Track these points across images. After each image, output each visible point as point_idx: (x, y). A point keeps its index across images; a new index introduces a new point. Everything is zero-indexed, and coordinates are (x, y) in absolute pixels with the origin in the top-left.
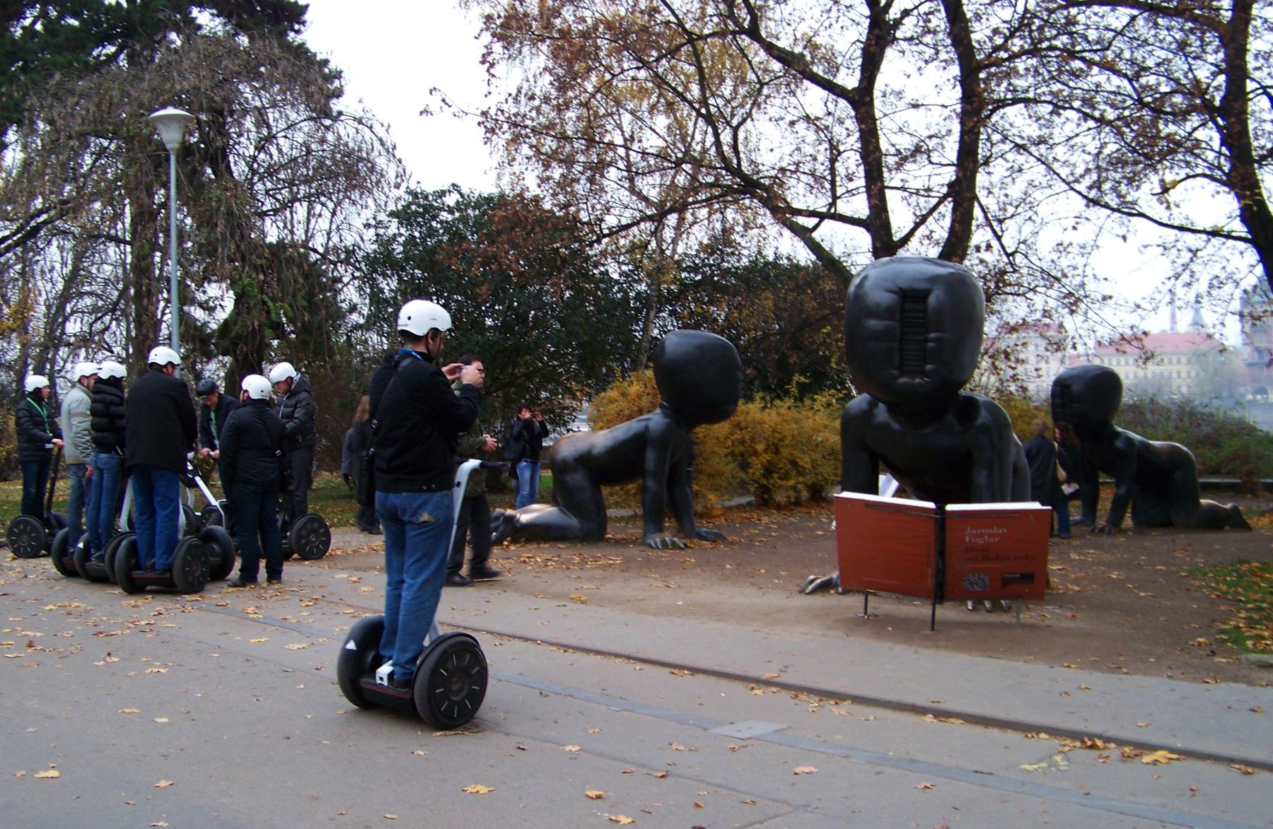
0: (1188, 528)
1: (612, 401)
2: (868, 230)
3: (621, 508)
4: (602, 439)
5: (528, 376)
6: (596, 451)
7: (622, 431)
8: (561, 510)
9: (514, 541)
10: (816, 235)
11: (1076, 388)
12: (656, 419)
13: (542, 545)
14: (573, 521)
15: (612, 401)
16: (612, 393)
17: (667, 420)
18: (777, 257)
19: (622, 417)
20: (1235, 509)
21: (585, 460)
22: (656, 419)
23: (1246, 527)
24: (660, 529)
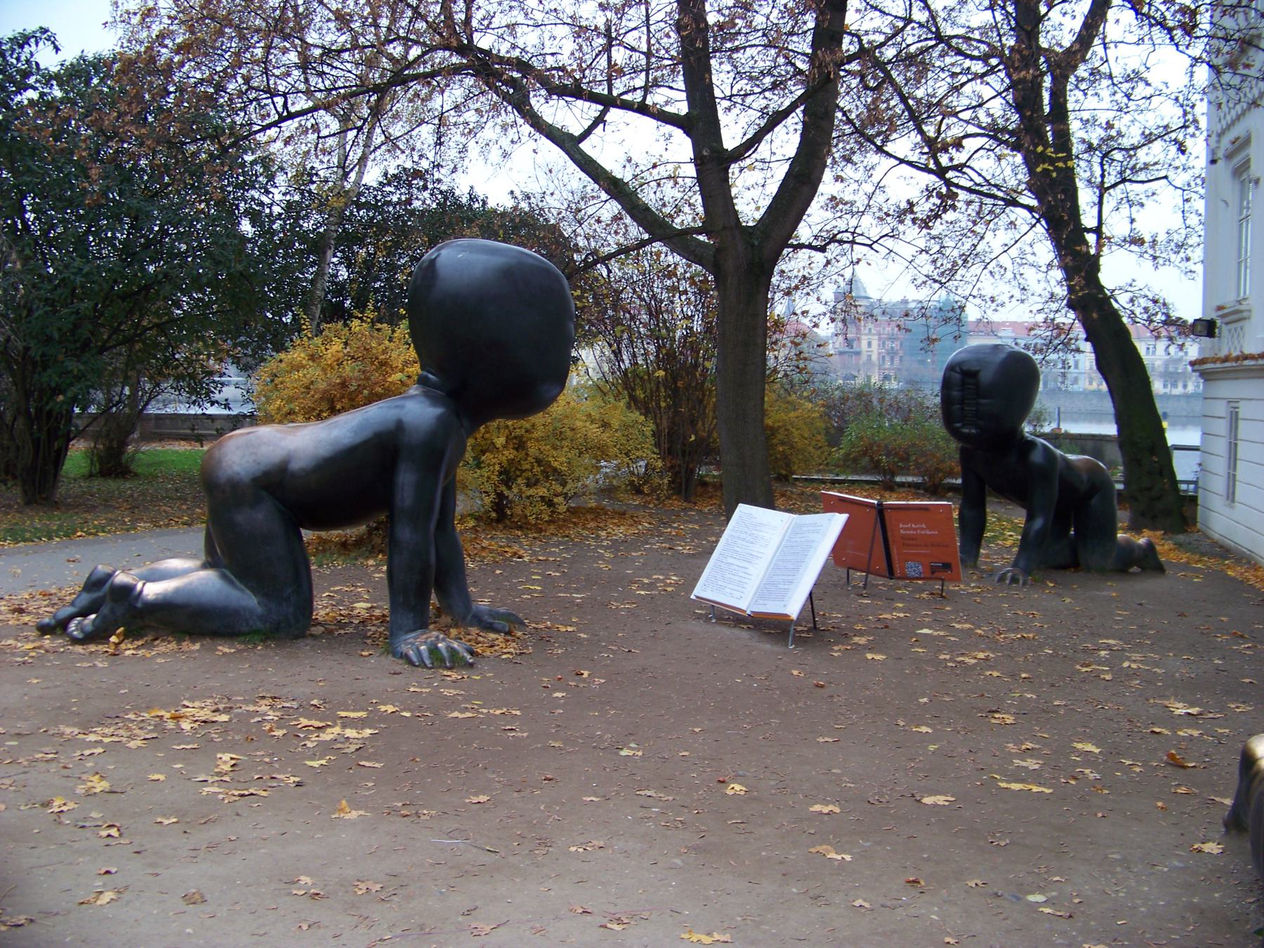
0: (1103, 572)
1: (298, 367)
2: (687, 133)
3: (350, 586)
4: (305, 441)
5: (161, 328)
6: (296, 466)
7: (341, 430)
8: (224, 577)
9: (131, 635)
10: (585, 146)
11: (986, 376)
12: (417, 410)
13: (186, 646)
14: (246, 599)
15: (298, 367)
16: (296, 355)
17: (438, 411)
18: (473, 198)
19: (330, 404)
20: (1150, 547)
21: (276, 483)
22: (417, 410)
23: (1159, 569)
24: (422, 624)
